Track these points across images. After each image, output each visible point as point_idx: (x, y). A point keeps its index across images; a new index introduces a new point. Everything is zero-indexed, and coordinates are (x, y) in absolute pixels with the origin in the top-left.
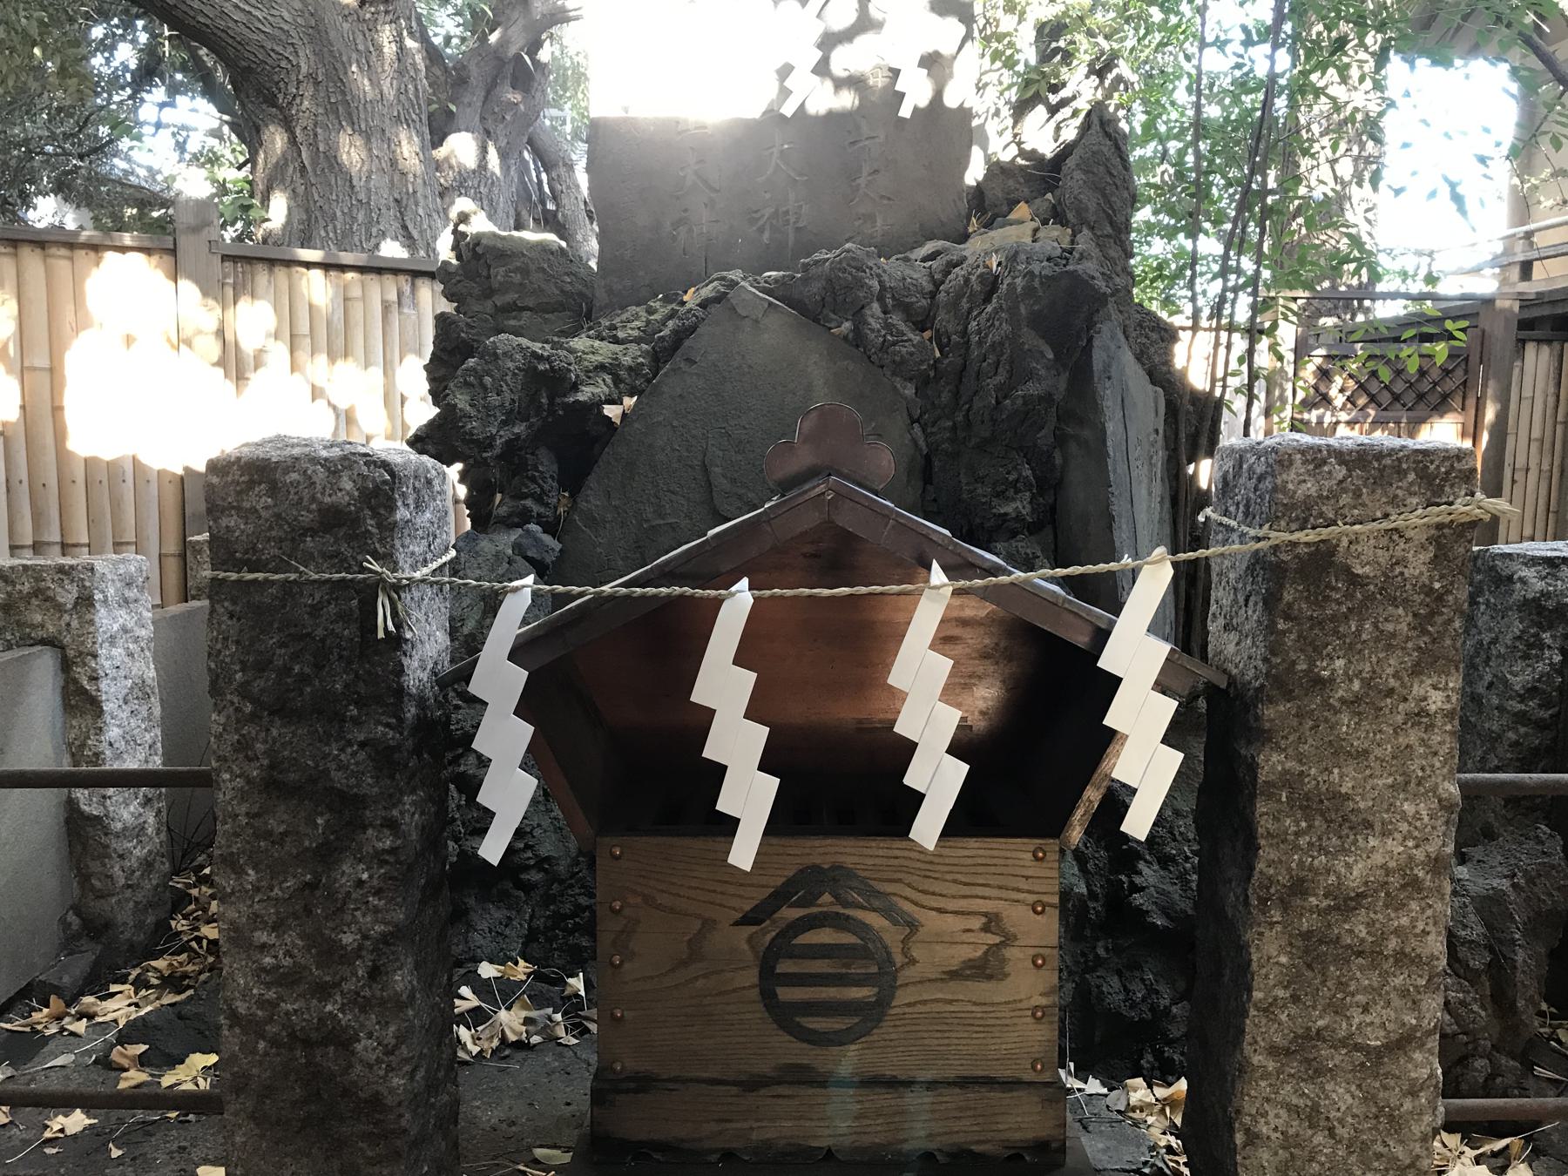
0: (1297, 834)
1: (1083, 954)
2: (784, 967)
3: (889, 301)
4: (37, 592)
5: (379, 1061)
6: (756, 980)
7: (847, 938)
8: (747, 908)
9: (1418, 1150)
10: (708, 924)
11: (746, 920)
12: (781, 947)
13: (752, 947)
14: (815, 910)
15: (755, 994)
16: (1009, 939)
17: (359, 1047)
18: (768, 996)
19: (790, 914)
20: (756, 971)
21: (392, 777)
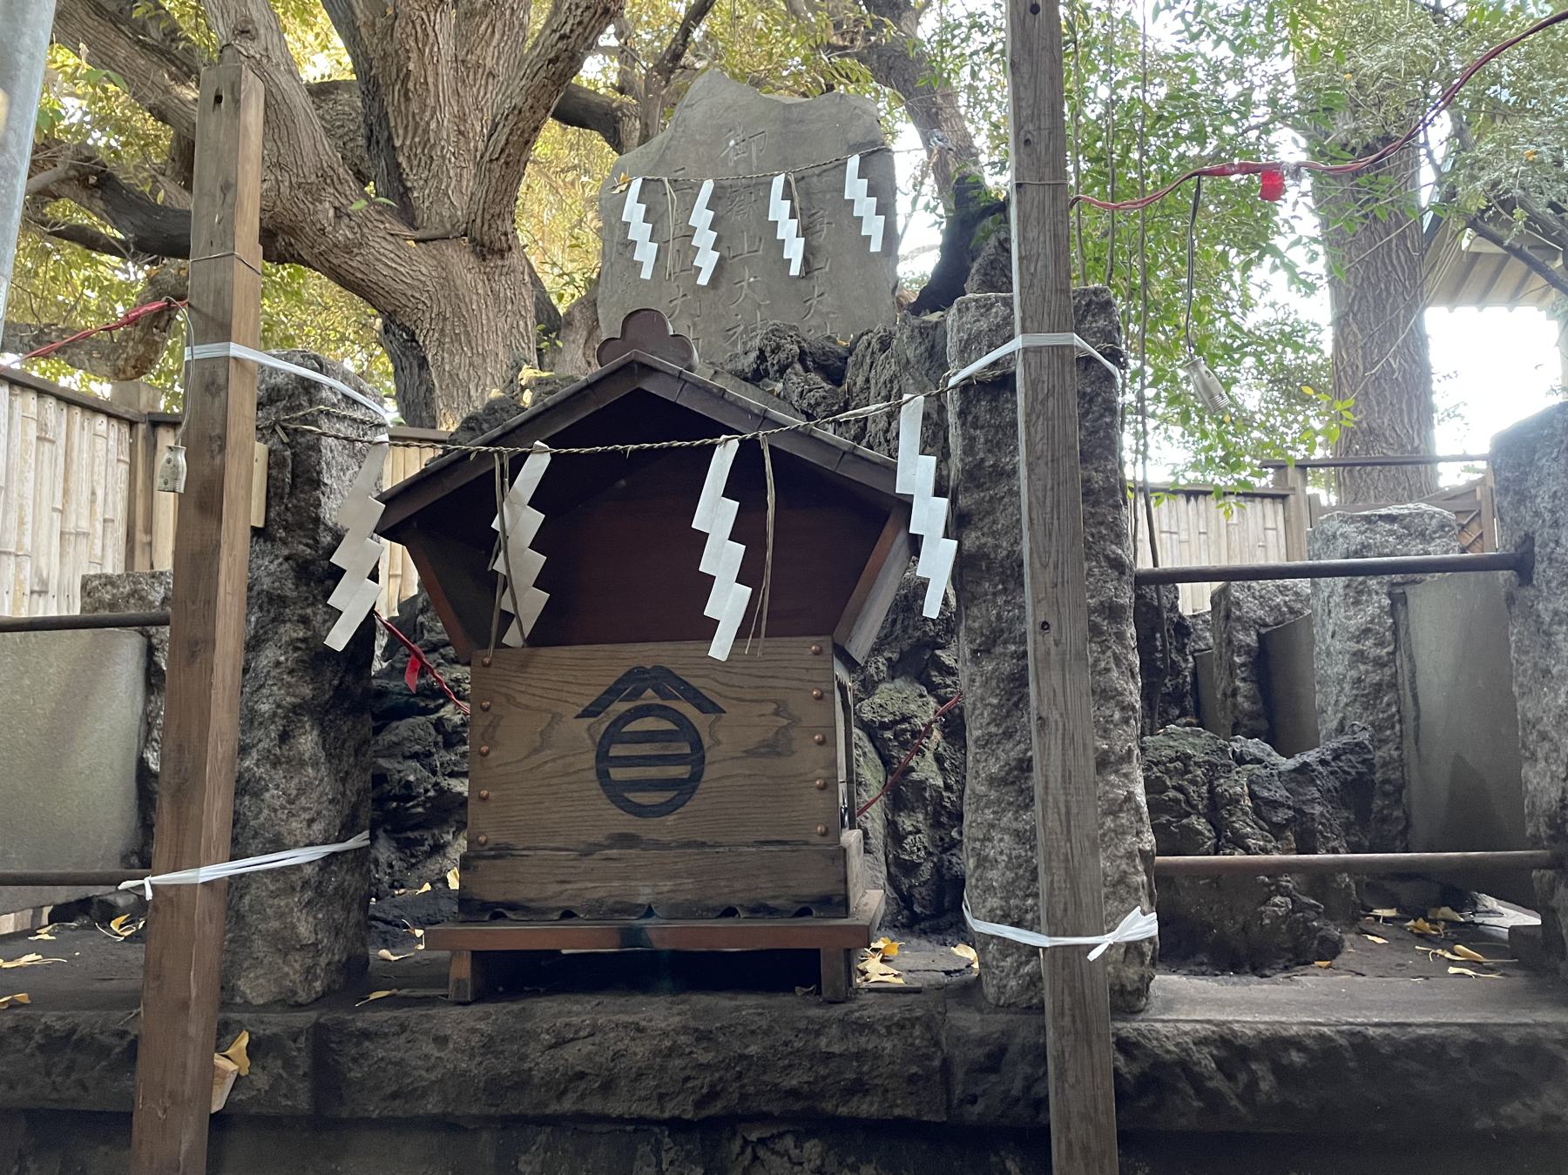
0: (994, 594)
1: (942, 839)
2: (616, 751)
3: (810, 364)
4: (133, 593)
5: (283, 807)
6: (593, 762)
7: (667, 725)
8: (587, 704)
9: (1124, 866)
10: (556, 718)
11: (586, 714)
12: (613, 734)
13: (591, 736)
14: (639, 703)
15: (592, 775)
16: (795, 721)
17: (267, 795)
18: (603, 775)
19: (620, 707)
20: (593, 755)
21: (308, 585)
